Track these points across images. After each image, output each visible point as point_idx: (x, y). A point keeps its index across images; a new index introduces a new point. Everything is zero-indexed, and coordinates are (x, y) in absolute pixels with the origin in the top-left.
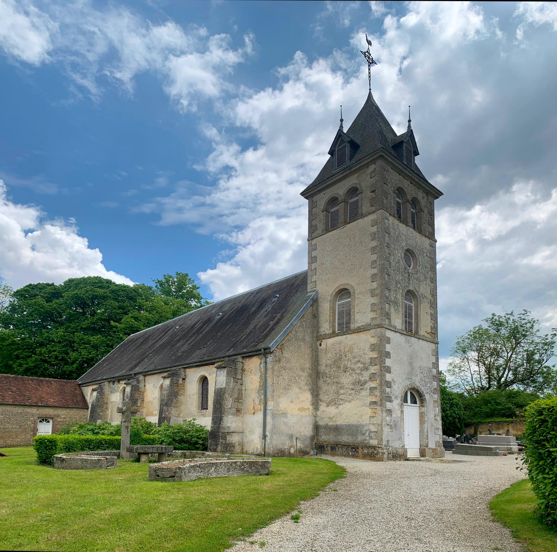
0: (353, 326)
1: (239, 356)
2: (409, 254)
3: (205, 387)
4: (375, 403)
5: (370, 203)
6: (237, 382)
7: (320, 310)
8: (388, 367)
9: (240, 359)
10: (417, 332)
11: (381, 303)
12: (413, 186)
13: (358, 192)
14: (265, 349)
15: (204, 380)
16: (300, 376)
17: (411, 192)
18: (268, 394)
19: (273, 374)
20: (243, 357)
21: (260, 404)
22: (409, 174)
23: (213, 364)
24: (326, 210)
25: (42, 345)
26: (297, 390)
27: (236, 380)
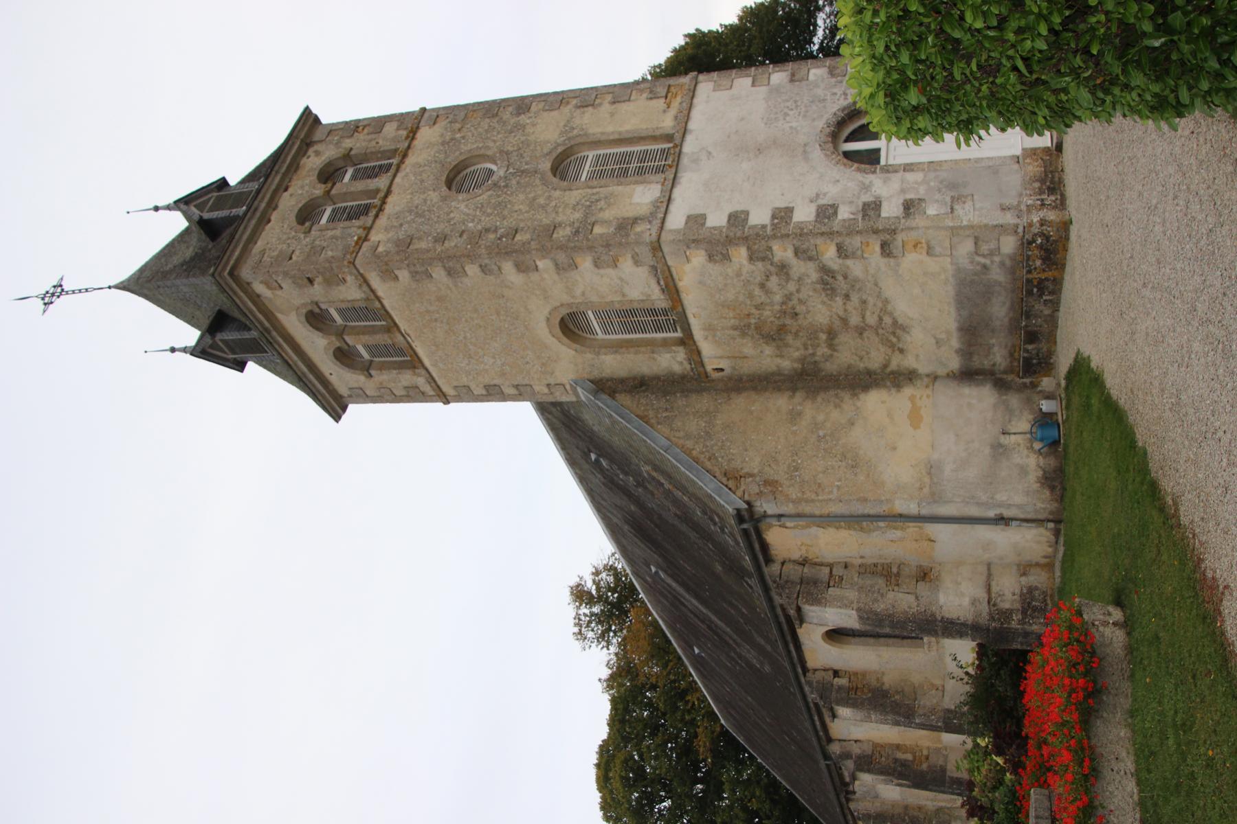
1: (766, 570)
2: (457, 178)
5: (338, 285)
6: (841, 578)
8: (774, 217)
9: (775, 568)
10: (669, 138)
11: (591, 248)
12: (293, 183)
13: (317, 310)
15: (836, 635)
17: (307, 188)
18: (872, 512)
19: (813, 501)
20: (769, 560)
22: (266, 200)
24: (367, 369)
26: (857, 434)
27: (834, 580)
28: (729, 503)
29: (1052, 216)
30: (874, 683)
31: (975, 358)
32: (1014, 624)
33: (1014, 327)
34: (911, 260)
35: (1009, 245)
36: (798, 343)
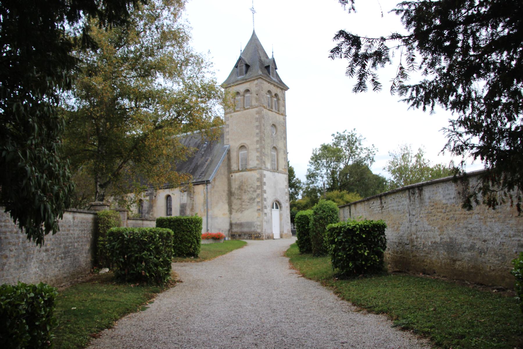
3: (168, 202)
4: (259, 210)
7: (231, 156)
10: (278, 169)
11: (261, 156)
14: (207, 181)
15: (168, 197)
20: (194, 185)
28: (210, 179)
29: (264, 237)
30: (154, 205)
33: (242, 232)
34: (256, 214)
35: (259, 231)
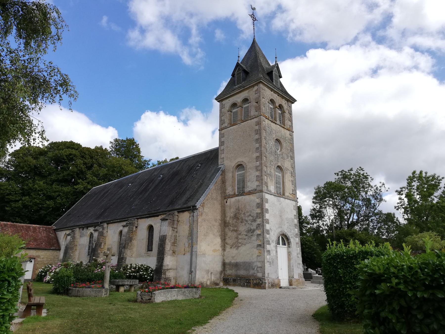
0: (247, 190)
1: (176, 211)
4: (260, 245)
7: (226, 177)
10: (284, 194)
13: (249, 102)
14: (193, 207)
15: (151, 228)
16: (214, 226)
20: (179, 212)
21: (188, 247)
23: (158, 216)
25: (84, 217)
29: (267, 285)
30: (134, 238)
31: (229, 266)
32: (163, 276)
33: (237, 276)
35: (260, 275)
36: (234, 222)
